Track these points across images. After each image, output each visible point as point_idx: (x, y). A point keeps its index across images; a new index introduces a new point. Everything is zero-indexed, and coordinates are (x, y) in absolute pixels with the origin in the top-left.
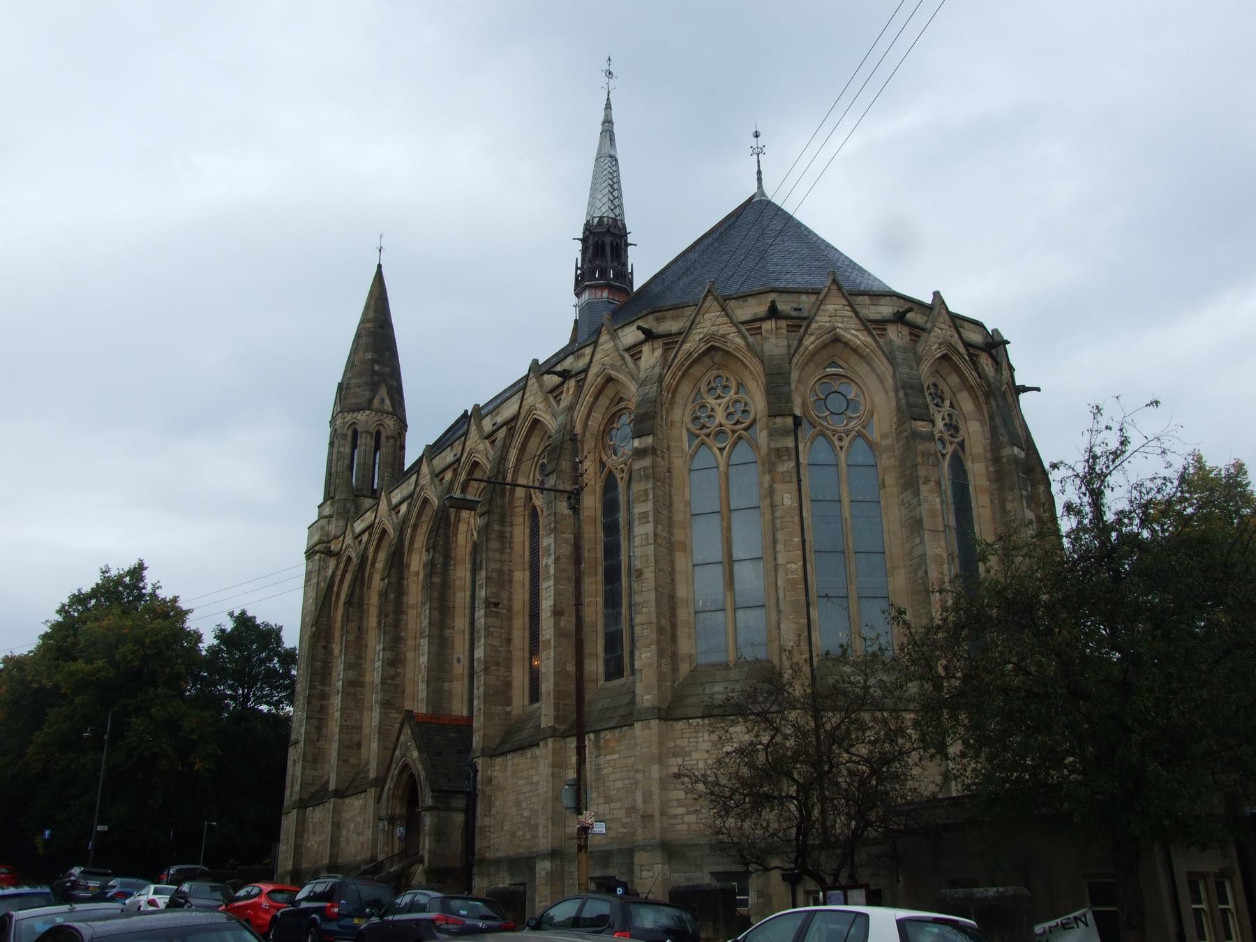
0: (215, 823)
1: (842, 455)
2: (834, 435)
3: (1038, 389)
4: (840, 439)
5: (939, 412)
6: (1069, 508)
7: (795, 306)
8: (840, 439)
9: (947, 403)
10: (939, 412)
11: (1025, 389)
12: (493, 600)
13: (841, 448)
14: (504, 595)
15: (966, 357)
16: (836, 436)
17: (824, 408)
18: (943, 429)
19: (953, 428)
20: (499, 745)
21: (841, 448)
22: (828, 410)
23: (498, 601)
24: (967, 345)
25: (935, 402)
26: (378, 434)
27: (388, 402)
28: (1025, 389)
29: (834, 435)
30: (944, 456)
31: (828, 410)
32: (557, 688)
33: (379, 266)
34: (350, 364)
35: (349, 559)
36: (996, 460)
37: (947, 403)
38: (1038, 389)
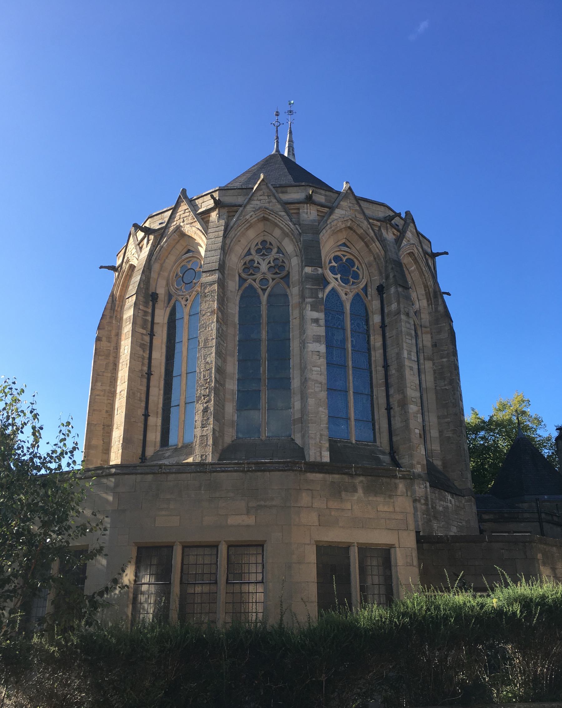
3: (446, 253)
9: (275, 250)
10: (264, 260)
15: (283, 213)
17: (182, 282)
21: (186, 305)
24: (285, 204)
29: (182, 298)
38: (446, 253)
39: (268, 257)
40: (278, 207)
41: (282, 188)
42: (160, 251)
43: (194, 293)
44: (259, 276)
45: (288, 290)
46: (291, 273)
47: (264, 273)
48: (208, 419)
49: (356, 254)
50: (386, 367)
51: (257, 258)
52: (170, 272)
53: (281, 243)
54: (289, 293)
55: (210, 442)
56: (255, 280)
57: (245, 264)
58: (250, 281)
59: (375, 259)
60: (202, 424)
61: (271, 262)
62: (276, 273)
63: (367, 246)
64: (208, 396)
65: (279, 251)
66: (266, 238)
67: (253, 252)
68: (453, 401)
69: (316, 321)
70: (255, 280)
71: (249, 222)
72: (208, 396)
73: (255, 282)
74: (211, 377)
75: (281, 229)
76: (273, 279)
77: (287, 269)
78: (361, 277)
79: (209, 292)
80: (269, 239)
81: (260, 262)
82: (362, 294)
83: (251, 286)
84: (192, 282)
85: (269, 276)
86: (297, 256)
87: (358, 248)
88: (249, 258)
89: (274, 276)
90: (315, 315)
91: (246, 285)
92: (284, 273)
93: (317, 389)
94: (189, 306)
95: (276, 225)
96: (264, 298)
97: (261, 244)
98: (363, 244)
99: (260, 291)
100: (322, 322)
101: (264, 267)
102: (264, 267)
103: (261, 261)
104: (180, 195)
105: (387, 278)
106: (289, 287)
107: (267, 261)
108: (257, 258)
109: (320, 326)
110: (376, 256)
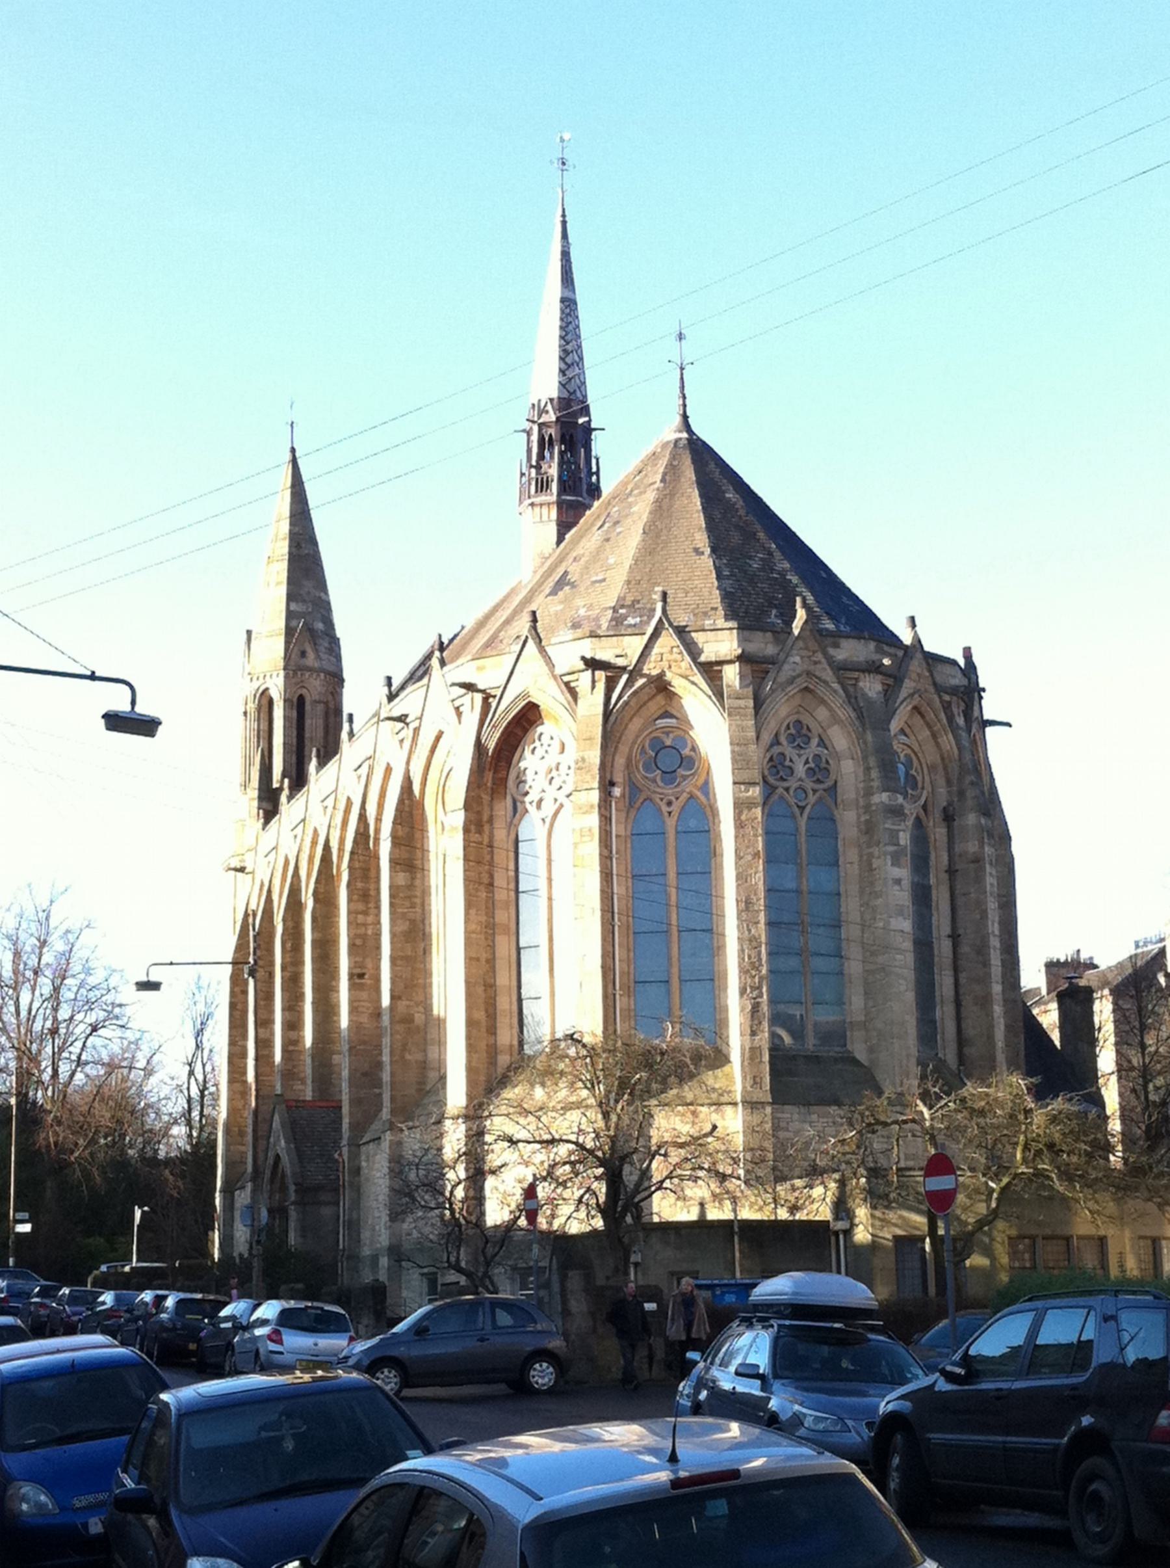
0: (138, 1214)
1: (671, 823)
2: (662, 799)
3: (1009, 725)
4: (669, 804)
5: (800, 756)
6: (825, 669)
7: (619, 652)
8: (669, 804)
9: (815, 741)
10: (800, 756)
11: (595, 429)
12: (358, 971)
13: (670, 813)
14: (369, 964)
15: (836, 686)
16: (664, 801)
18: (804, 776)
19: (820, 770)
20: (270, 1198)
21: (670, 813)
22: (658, 768)
23: (364, 971)
25: (796, 744)
26: (301, 700)
27: (311, 655)
28: (595, 429)
29: (662, 799)
30: (802, 809)
31: (658, 768)
32: (377, 1091)
33: (293, 450)
34: (341, 695)
35: (388, 770)
36: (867, 808)
37: (815, 741)
38: (1009, 725)
39: (807, 751)
40: (828, 675)
41: (835, 637)
42: (623, 708)
43: (685, 795)
44: (793, 784)
45: (836, 812)
46: (839, 784)
47: (801, 780)
48: (760, 1023)
49: (916, 748)
50: (955, 937)
51: (789, 751)
52: (634, 743)
53: (825, 731)
54: (837, 817)
55: (766, 1057)
56: (787, 789)
57: (771, 759)
58: (780, 790)
59: (943, 759)
60: (752, 1031)
61: (810, 760)
62: (819, 781)
63: (934, 736)
64: (758, 988)
65: (822, 743)
66: (802, 718)
67: (783, 739)
68: (1012, 980)
69: (898, 882)
70: (787, 789)
71: (786, 694)
72: (758, 988)
73: (788, 793)
74: (760, 960)
75: (830, 709)
76: (815, 791)
77: (833, 777)
78: (920, 785)
79: (747, 820)
80: (806, 719)
81: (794, 759)
82: (922, 812)
83: (781, 797)
84: (675, 771)
85: (809, 785)
86: (853, 759)
87: (920, 738)
88: (776, 750)
89: (817, 786)
90: (897, 872)
91: (775, 797)
92: (829, 783)
93: (903, 988)
94: (675, 815)
95: (823, 702)
96: (803, 822)
97: (794, 726)
98: (928, 733)
99: (796, 810)
100: (906, 883)
101: (800, 769)
102: (800, 769)
103: (795, 758)
104: (660, 618)
105: (961, 794)
106: (837, 808)
107: (804, 758)
108: (789, 751)
109: (902, 890)
110: (946, 756)
